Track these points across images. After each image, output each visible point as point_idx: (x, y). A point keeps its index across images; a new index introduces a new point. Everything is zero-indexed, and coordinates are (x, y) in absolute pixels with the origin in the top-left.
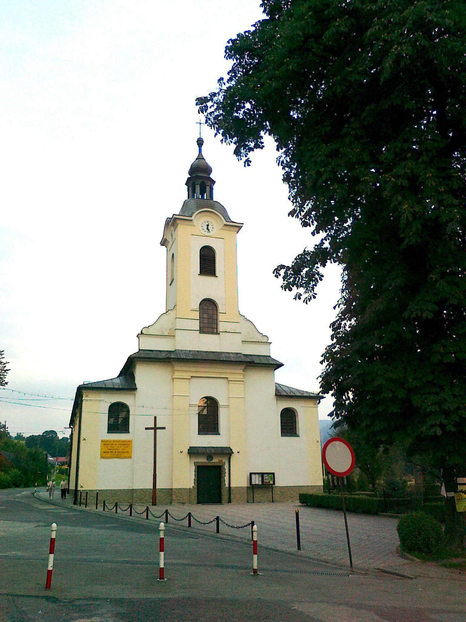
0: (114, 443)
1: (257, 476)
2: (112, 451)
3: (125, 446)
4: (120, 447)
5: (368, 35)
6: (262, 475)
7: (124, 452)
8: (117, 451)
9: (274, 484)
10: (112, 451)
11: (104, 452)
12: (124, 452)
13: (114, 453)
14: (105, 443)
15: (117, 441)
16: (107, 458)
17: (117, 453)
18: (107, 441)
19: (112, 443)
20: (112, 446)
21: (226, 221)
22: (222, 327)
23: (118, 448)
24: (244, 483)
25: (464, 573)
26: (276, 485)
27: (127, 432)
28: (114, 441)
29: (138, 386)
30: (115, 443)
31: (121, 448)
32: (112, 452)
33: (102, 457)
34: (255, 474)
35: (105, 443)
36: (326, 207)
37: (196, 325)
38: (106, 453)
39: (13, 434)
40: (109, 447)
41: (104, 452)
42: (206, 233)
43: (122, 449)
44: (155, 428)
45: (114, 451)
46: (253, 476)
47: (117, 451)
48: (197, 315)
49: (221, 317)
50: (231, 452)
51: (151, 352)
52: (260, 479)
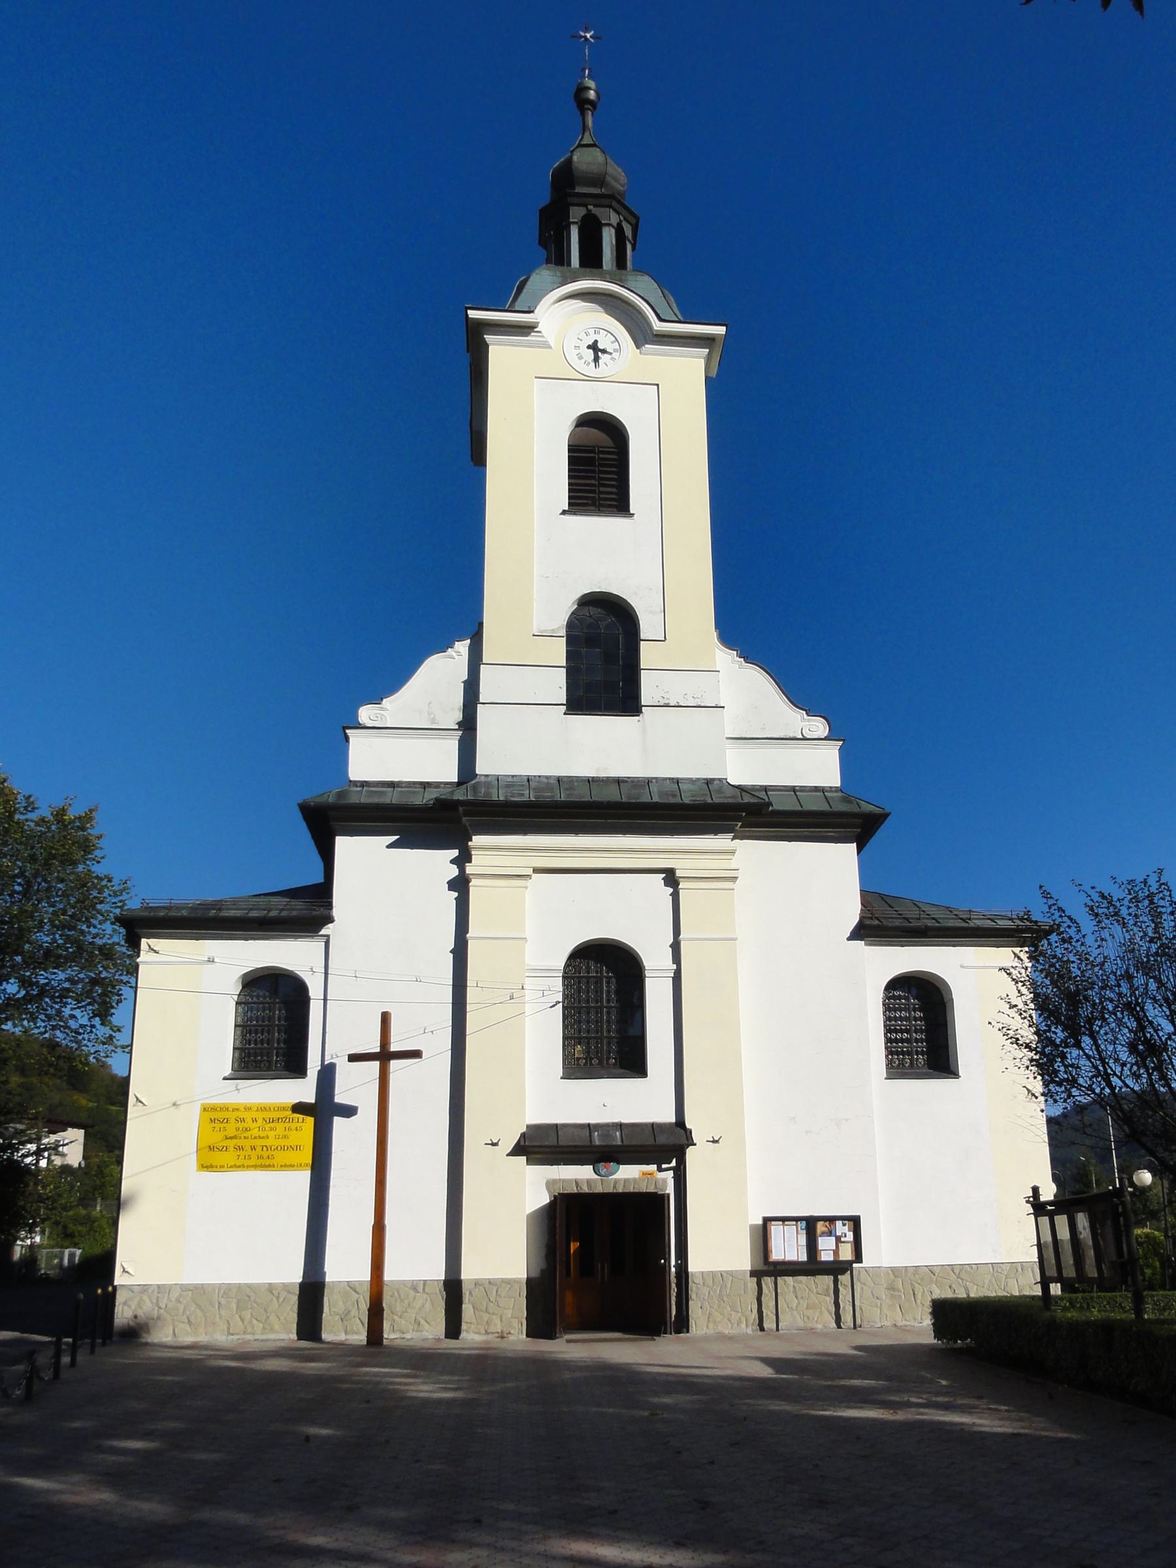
0: (248, 1116)
1: (791, 1229)
2: (240, 1142)
3: (287, 1125)
4: (271, 1129)
5: (1130, 1208)
6: (810, 1224)
7: (283, 1148)
8: (259, 1143)
9: (858, 1257)
10: (240, 1142)
11: (211, 1148)
12: (283, 1148)
13: (249, 1152)
14: (214, 1115)
15: (263, 1109)
16: (221, 1168)
17: (259, 1149)
18: (225, 1108)
19: (242, 1115)
20: (241, 1125)
21: (661, 320)
22: (650, 687)
23: (262, 1134)
24: (742, 1260)
25: (101, 874)
26: (868, 1260)
27: (666, 1198)
28: (248, 1109)
29: (336, 912)
30: (254, 1115)
31: (272, 1134)
32: (241, 1148)
33: (205, 1167)
34: (784, 1220)
35: (214, 1115)
36: (1115, 1199)
37: (556, 685)
38: (217, 1153)
39: (70, 1129)
40: (231, 1130)
41: (211, 1148)
42: (591, 370)
43: (277, 1137)
44: (385, 1056)
45: (247, 1144)
46: (775, 1229)
47: (259, 1143)
48: (558, 651)
49: (648, 655)
50: (684, 1141)
51: (390, 789)
52: (803, 1240)
